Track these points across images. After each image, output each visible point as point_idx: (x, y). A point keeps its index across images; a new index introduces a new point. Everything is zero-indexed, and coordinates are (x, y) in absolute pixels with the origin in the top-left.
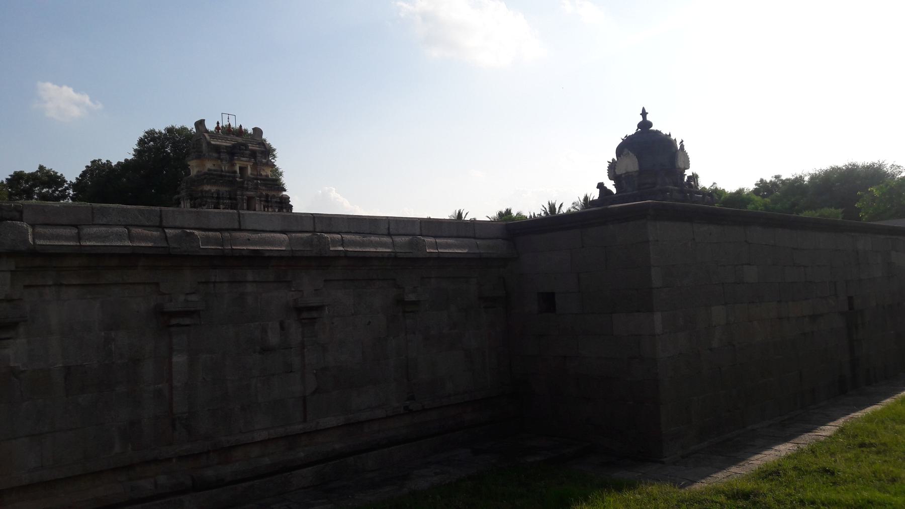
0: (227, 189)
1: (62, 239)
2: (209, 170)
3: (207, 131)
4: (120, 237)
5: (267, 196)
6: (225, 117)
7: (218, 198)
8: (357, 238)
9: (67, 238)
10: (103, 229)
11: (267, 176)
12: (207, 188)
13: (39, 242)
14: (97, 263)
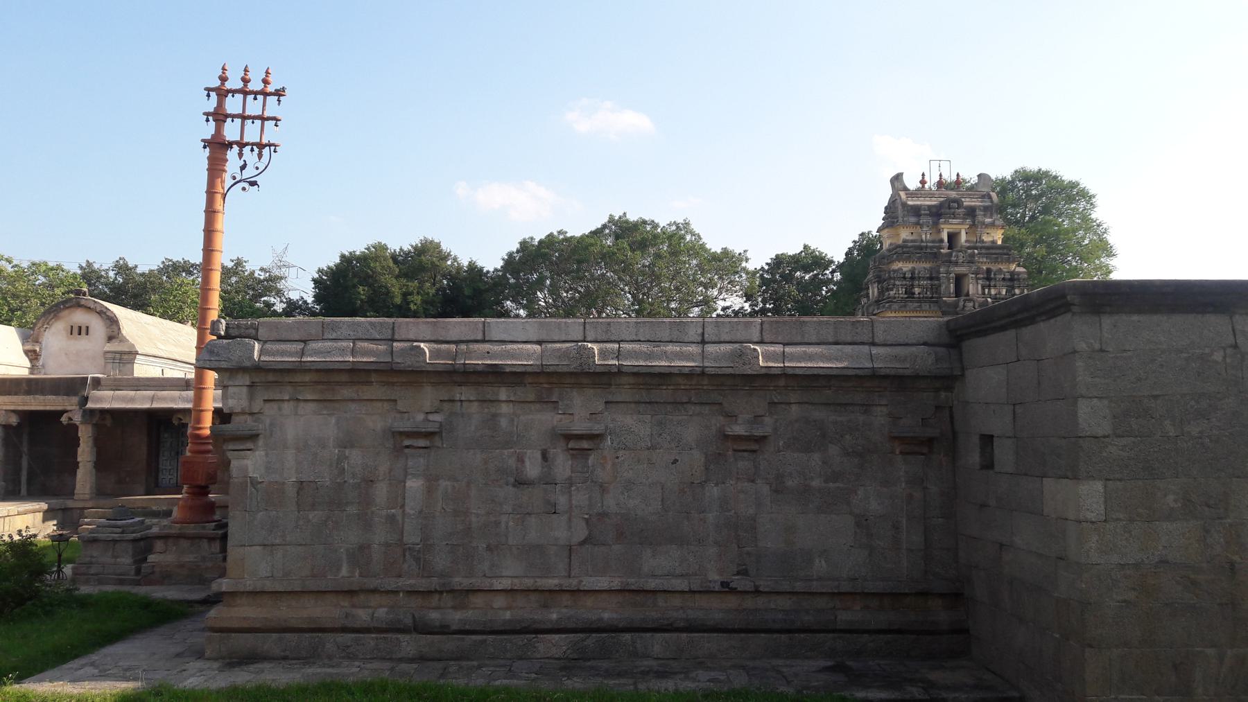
0: (927, 265)
1: (286, 355)
2: (905, 241)
3: (905, 189)
4: (343, 351)
5: (989, 271)
6: (935, 165)
7: (912, 278)
8: (644, 347)
9: (291, 355)
10: (330, 344)
11: (994, 242)
12: (897, 265)
13: (263, 358)
14: (329, 380)
